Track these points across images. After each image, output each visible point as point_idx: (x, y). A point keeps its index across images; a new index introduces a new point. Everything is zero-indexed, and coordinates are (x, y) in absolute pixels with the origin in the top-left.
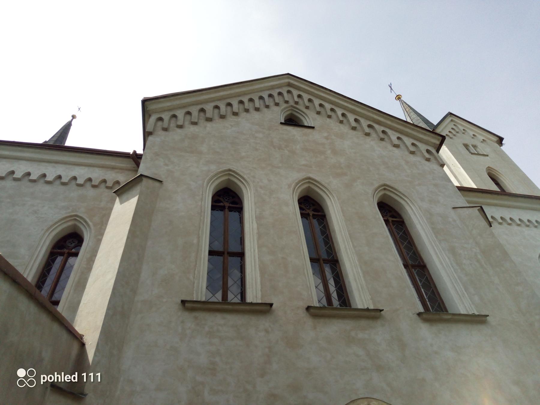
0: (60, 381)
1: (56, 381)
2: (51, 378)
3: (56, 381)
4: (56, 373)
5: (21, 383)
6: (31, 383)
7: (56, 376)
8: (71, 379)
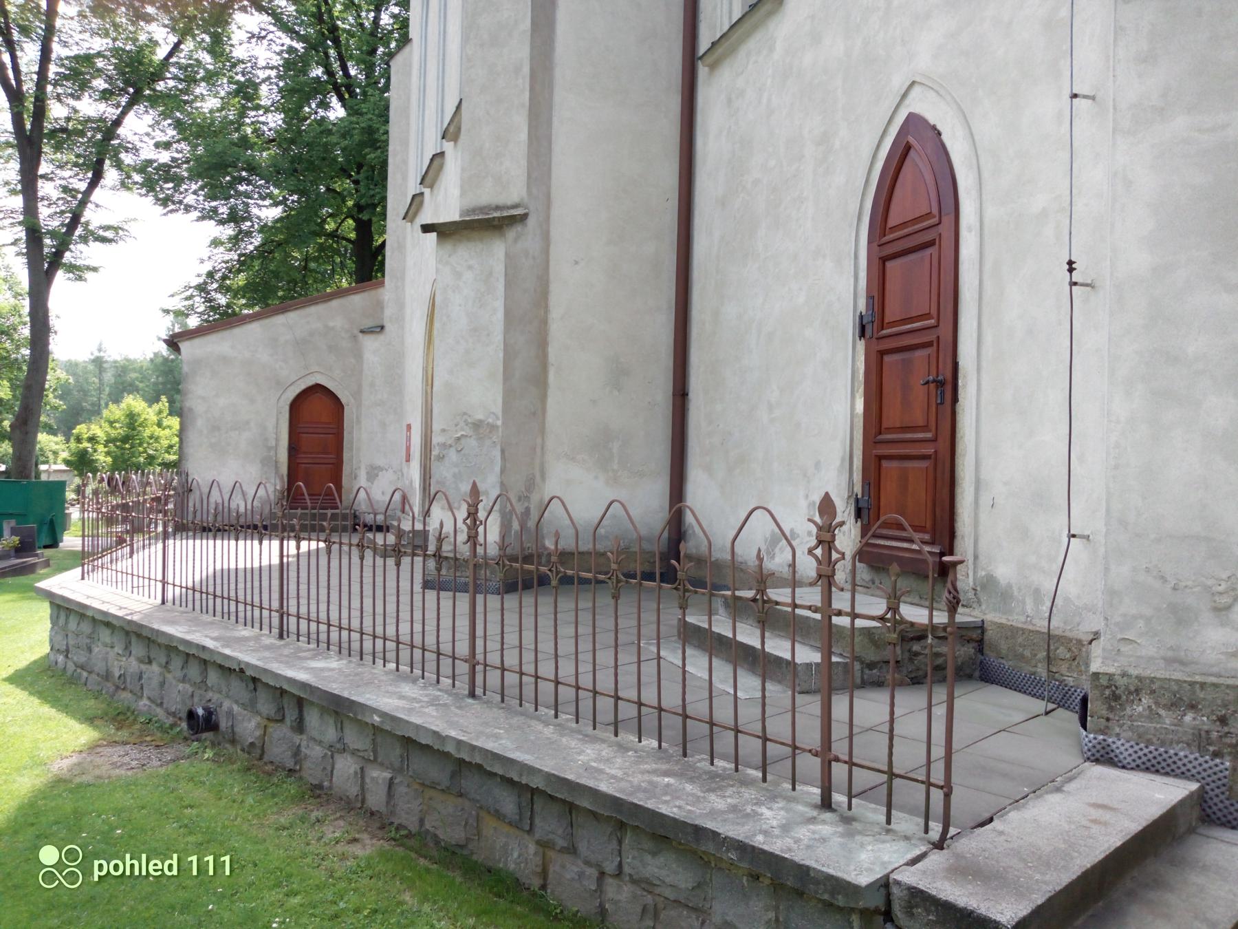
0: (137, 873)
1: (128, 873)
2: (116, 867)
4: (128, 856)
5: (49, 877)
6: (72, 877)
7: (128, 863)
8: (162, 870)
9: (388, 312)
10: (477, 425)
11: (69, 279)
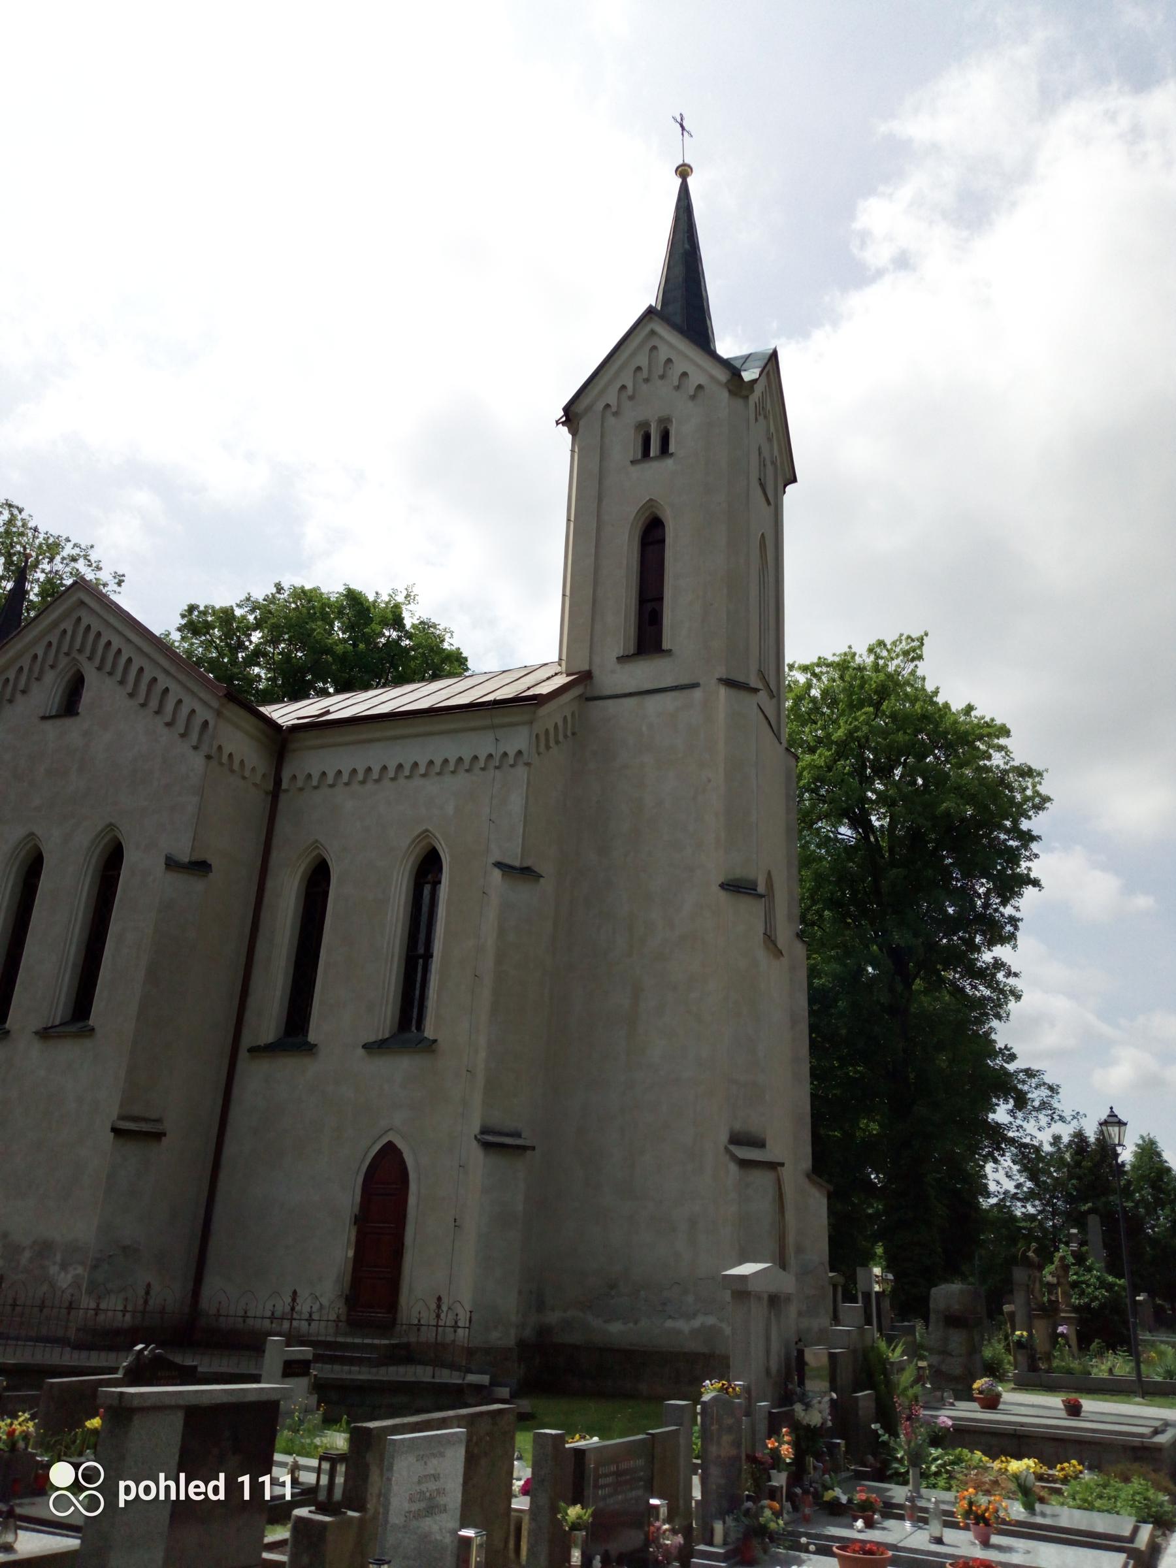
0: (173, 1497)
1: (162, 1497)
2: (147, 1490)
3: (162, 1497)
4: (162, 1476)
7: (162, 1484)
8: (205, 1494)
10: (125, 1249)
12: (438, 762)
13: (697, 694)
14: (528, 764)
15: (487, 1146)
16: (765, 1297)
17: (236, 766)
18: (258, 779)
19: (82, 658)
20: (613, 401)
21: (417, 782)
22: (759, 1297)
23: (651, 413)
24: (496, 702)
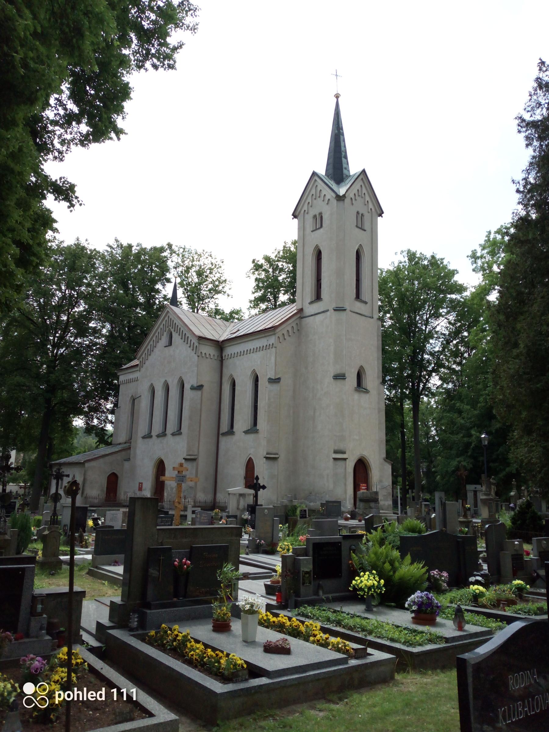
0: (81, 699)
1: (76, 699)
2: (69, 696)
3: (76, 699)
4: (76, 689)
7: (76, 693)
8: (96, 697)
9: (131, 456)
11: (490, 233)
12: (265, 346)
13: (328, 313)
14: (275, 347)
15: (267, 458)
16: (238, 495)
17: (208, 356)
18: (216, 358)
19: (171, 328)
20: (306, 209)
21: (252, 354)
22: (235, 494)
23: (314, 211)
24: (265, 329)
